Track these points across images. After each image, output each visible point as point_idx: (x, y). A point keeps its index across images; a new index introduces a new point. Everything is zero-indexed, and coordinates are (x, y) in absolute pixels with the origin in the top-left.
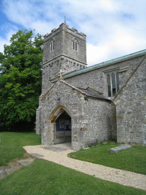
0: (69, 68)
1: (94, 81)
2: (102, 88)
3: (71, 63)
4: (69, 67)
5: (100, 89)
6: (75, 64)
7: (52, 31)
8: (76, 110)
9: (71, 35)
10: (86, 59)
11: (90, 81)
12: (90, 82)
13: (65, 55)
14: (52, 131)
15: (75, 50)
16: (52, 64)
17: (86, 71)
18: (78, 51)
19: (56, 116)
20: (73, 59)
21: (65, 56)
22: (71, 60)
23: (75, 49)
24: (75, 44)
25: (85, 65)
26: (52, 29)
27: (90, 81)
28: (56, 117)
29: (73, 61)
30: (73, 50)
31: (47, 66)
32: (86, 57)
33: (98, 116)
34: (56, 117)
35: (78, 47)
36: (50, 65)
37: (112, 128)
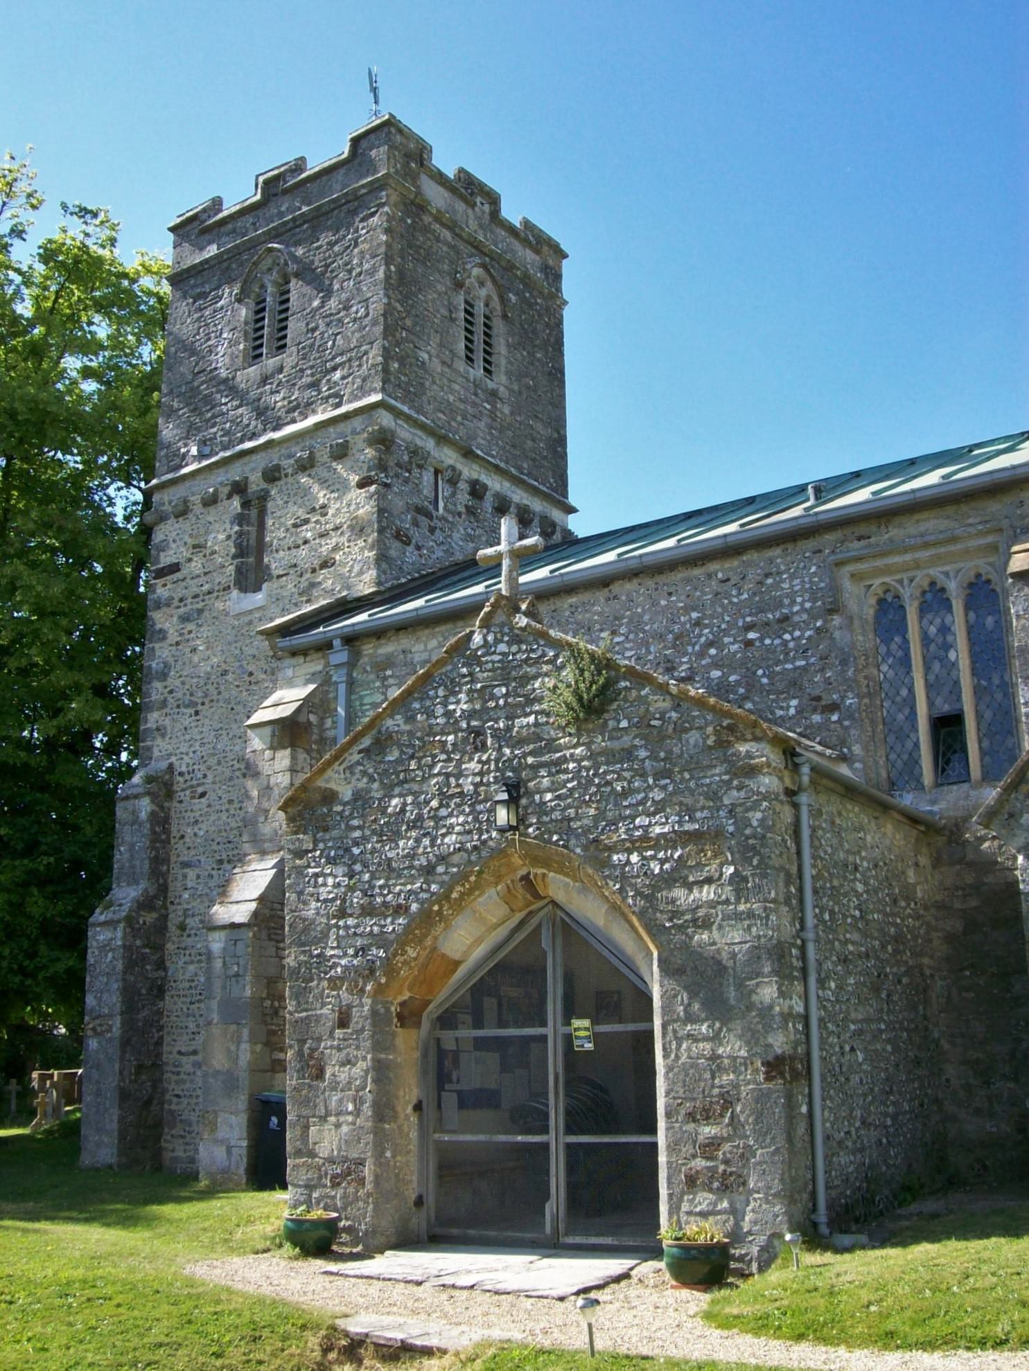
0: (432, 530)
1: (749, 643)
2: (833, 707)
3: (453, 482)
4: (429, 516)
5: (816, 718)
6: (477, 490)
7: (273, 187)
8: (708, 893)
9: (447, 235)
10: (564, 456)
11: (711, 644)
12: (702, 654)
13: (405, 409)
14: (409, 1109)
15: (478, 372)
16: (272, 475)
17: (925, 515)
18: (500, 382)
19: (457, 957)
20: (468, 454)
21: (408, 418)
22: (449, 457)
23: (479, 356)
24: (479, 329)
25: (556, 515)
26: (272, 160)
27: (711, 644)
28: (457, 964)
29: (470, 471)
30: (461, 365)
31: (211, 501)
32: (562, 441)
33: (867, 956)
34: (457, 964)
35: (500, 349)
36: (239, 488)
37: (950, 1071)
